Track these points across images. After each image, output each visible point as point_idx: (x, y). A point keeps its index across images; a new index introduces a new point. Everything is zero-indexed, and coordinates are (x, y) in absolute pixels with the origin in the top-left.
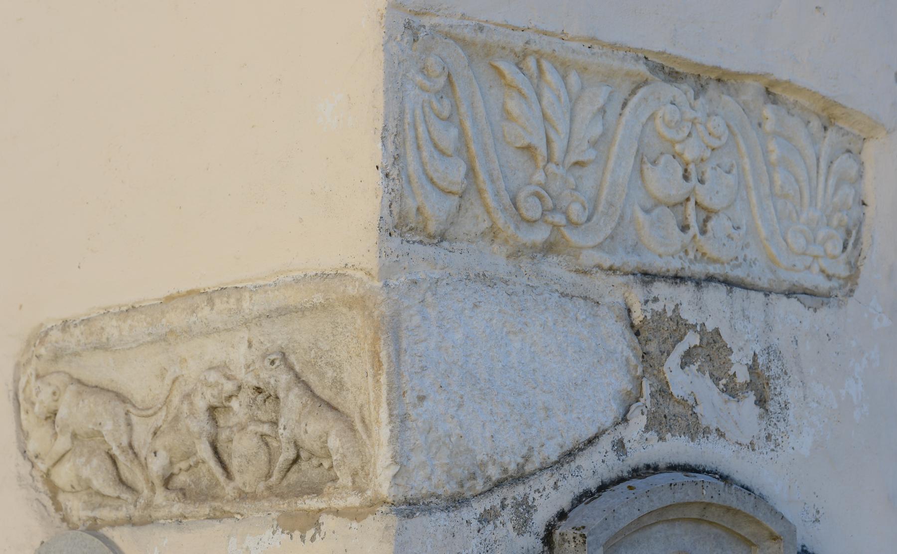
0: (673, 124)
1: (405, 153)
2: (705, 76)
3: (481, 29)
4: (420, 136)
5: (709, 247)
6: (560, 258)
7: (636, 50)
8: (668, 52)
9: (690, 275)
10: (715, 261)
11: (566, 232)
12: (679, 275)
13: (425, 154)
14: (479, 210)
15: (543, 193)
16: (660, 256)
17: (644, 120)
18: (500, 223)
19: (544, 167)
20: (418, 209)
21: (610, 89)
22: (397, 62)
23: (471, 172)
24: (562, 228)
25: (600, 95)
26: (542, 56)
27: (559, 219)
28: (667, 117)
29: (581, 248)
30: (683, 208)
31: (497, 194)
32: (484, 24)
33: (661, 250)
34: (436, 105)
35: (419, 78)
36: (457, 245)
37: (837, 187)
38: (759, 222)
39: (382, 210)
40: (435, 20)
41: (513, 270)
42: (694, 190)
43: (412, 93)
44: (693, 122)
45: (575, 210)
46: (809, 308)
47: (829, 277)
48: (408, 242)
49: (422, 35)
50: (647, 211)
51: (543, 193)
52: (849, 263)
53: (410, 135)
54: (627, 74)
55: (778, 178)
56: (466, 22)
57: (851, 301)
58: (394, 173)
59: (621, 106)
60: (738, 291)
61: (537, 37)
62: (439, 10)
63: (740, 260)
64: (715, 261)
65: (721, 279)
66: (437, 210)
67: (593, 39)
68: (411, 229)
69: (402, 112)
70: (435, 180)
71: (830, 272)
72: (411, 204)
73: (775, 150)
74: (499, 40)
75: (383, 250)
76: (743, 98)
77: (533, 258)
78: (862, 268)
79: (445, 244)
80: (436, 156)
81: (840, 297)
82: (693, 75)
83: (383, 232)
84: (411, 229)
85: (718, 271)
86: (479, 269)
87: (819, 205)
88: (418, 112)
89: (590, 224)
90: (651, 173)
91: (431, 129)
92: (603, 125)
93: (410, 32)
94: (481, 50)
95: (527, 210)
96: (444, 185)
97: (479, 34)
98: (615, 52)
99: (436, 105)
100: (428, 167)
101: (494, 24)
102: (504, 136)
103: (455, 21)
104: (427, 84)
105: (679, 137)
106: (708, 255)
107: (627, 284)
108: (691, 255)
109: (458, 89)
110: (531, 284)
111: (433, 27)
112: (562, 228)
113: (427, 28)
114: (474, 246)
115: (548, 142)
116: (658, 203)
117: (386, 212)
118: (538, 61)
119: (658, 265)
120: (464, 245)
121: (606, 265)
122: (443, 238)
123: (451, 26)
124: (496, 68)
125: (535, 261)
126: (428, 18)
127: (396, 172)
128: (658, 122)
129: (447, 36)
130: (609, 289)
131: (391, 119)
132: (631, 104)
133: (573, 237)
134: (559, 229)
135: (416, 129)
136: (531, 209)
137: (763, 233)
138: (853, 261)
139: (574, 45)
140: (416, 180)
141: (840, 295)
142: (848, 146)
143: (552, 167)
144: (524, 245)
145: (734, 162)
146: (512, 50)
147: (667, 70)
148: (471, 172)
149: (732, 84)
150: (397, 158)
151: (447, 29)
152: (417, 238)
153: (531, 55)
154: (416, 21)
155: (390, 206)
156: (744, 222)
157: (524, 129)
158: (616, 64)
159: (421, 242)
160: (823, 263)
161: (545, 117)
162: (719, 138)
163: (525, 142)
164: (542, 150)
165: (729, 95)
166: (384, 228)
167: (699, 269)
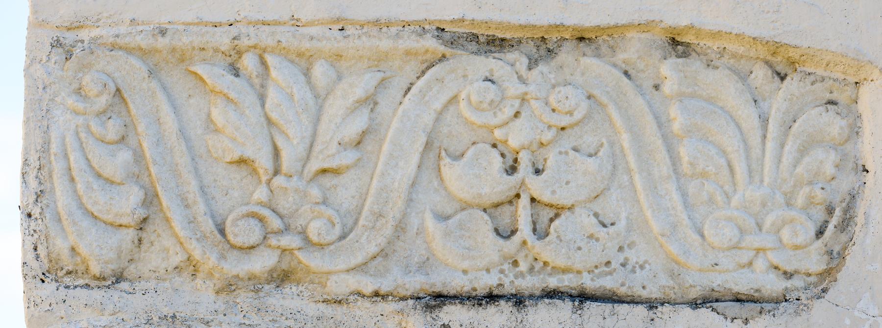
0: (485, 105)
1: (53, 189)
2: (554, 37)
3: (163, 32)
4: (72, 166)
5: (546, 251)
6: (301, 288)
7: (418, 23)
8: (469, 17)
9: (514, 292)
10: (565, 271)
11: (300, 255)
12: (495, 292)
13: (80, 186)
14: (167, 242)
15: (266, 212)
16: (465, 272)
17: (438, 105)
18: (197, 254)
19: (269, 182)
20: (73, 249)
21: (380, 75)
22: (41, 87)
23: (151, 199)
24: (296, 252)
25: (361, 84)
26: (264, 50)
27: (290, 241)
28: (474, 98)
29: (329, 273)
30: (512, 208)
31: (192, 221)
32: (167, 26)
33: (465, 265)
34: (95, 127)
35: (71, 101)
36: (139, 286)
37: (803, 151)
38: (648, 214)
39: (25, 254)
40: (95, 32)
41: (223, 307)
42: (523, 183)
43: (62, 118)
44: (523, 99)
45: (315, 230)
46: (733, 320)
47: (788, 275)
48: (67, 287)
49: (77, 51)
50: (443, 218)
51: (266, 212)
52: (830, 253)
53: (58, 167)
54: (408, 53)
55: (685, 152)
56: (140, 28)
57: (819, 306)
58: (36, 212)
59: (403, 93)
60: (592, 308)
61: (251, 30)
62: (98, 20)
63: (614, 265)
64: (565, 271)
65: (629, 299)
66: (99, 250)
67: (338, 20)
68: (69, 273)
69: (47, 143)
70: (95, 214)
71: (789, 269)
72: (61, 246)
73: (678, 119)
74: (191, 42)
75: (32, 299)
76: (621, 56)
77: (257, 291)
78: (848, 258)
79: (124, 285)
80: (95, 187)
81: (804, 301)
82: (533, 39)
83: (29, 280)
84: (69, 273)
85: (566, 283)
86: (167, 311)
87: (767, 180)
88: (70, 140)
89: (343, 242)
90: (451, 171)
91: (90, 157)
92: (370, 119)
93: (60, 50)
94: (166, 57)
95: (236, 235)
96: (109, 218)
97: (160, 39)
98: (385, 29)
99: (95, 127)
100: (84, 201)
101: (183, 24)
102: (209, 151)
103: (123, 30)
104: (80, 106)
105: (495, 121)
106: (551, 265)
107: (401, 312)
108: (523, 267)
109: (131, 106)
110: (247, 322)
111: (94, 40)
112: (296, 252)
113: (86, 42)
114: (167, 284)
115: (276, 153)
116: (465, 206)
117: (31, 255)
118: (261, 58)
119: (457, 283)
120: (152, 284)
121: (368, 290)
122: (119, 278)
123: (117, 36)
124: (196, 74)
125: (261, 294)
126: (87, 30)
127: (39, 210)
128: (463, 105)
129: (113, 47)
130: (375, 320)
131: (33, 152)
132: (414, 90)
133: (313, 261)
134: (292, 254)
135: (66, 156)
136: (244, 232)
137: (656, 227)
138: (837, 249)
139: (313, 31)
140: (66, 217)
141: (803, 297)
142: (828, 96)
143: (279, 181)
144: (237, 276)
145: (604, 141)
146: (216, 50)
147: (482, 39)
148: (151, 199)
149: (604, 40)
150: (39, 195)
151: (111, 40)
152: (81, 282)
153: (247, 51)
154: (69, 37)
155: (36, 249)
156: (624, 215)
157: (233, 140)
158: (385, 44)
159: (87, 286)
160: (774, 258)
161: (269, 122)
162: (570, 113)
163: (236, 156)
164: (264, 162)
165: (598, 56)
166: (30, 274)
167: (529, 284)
